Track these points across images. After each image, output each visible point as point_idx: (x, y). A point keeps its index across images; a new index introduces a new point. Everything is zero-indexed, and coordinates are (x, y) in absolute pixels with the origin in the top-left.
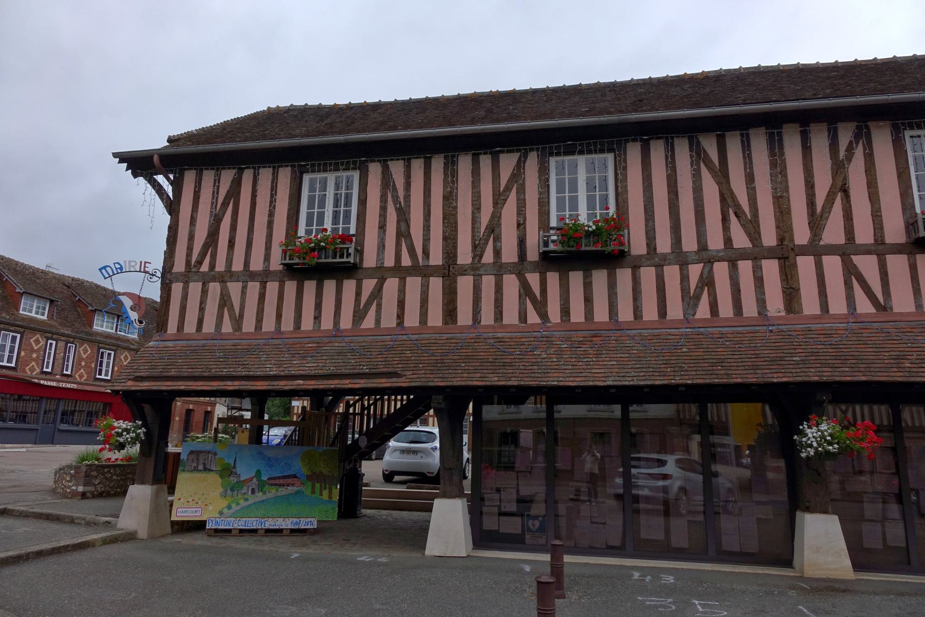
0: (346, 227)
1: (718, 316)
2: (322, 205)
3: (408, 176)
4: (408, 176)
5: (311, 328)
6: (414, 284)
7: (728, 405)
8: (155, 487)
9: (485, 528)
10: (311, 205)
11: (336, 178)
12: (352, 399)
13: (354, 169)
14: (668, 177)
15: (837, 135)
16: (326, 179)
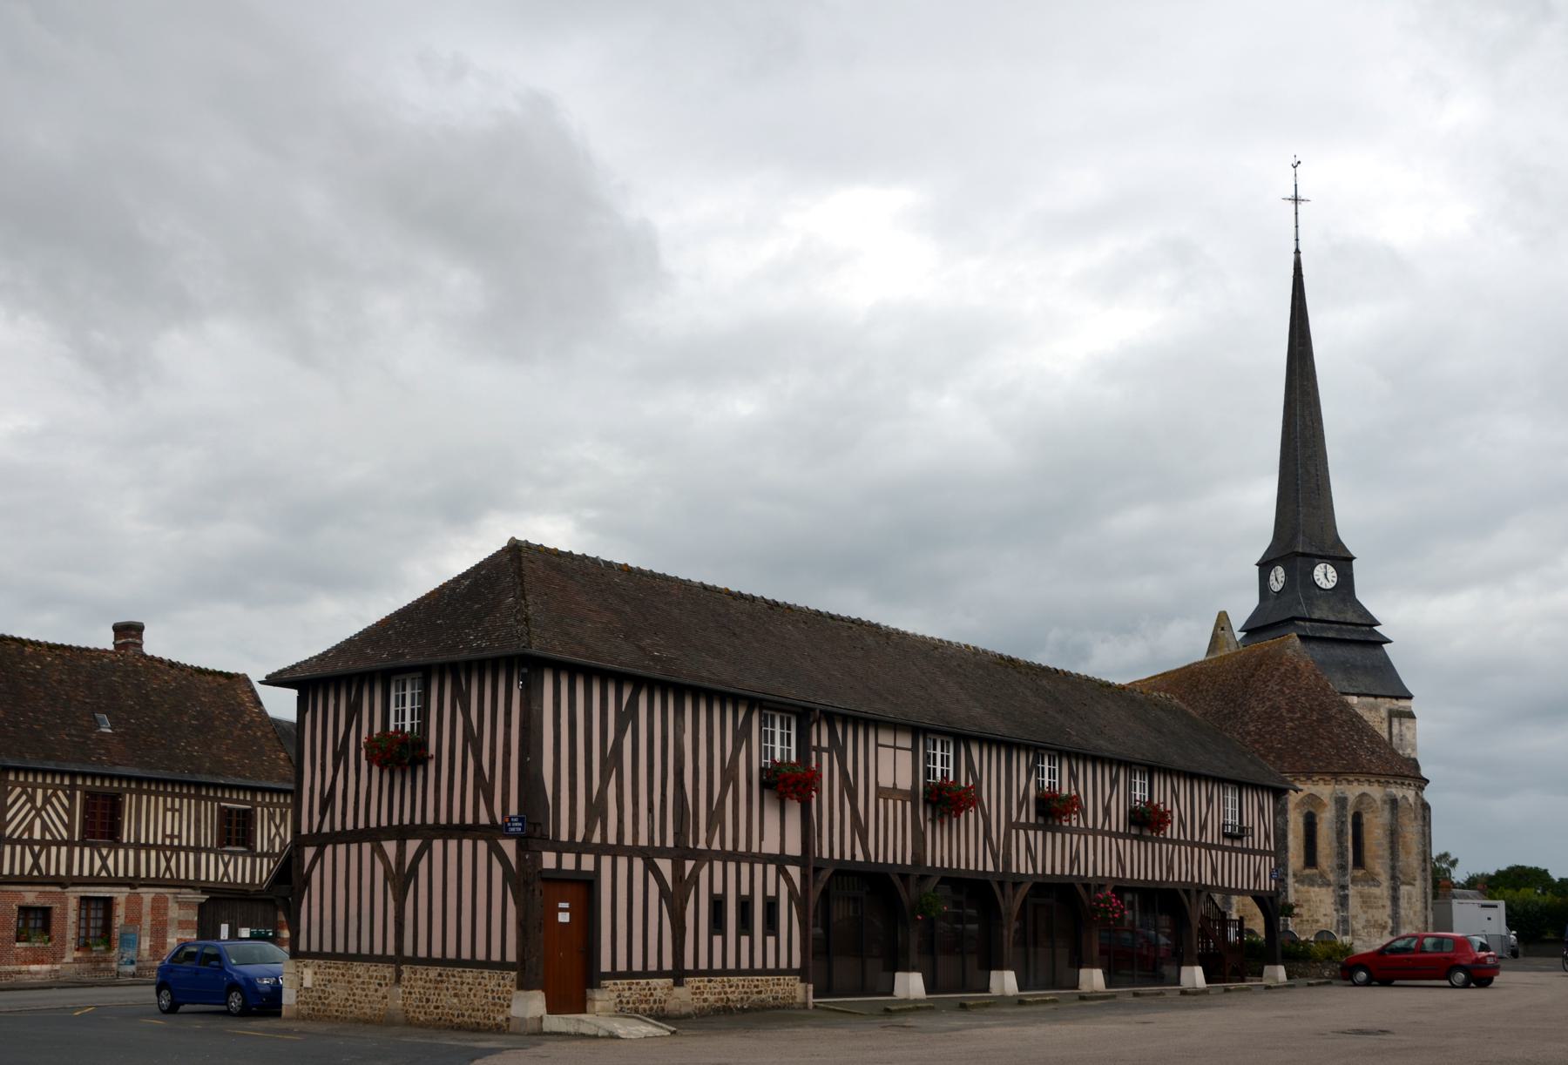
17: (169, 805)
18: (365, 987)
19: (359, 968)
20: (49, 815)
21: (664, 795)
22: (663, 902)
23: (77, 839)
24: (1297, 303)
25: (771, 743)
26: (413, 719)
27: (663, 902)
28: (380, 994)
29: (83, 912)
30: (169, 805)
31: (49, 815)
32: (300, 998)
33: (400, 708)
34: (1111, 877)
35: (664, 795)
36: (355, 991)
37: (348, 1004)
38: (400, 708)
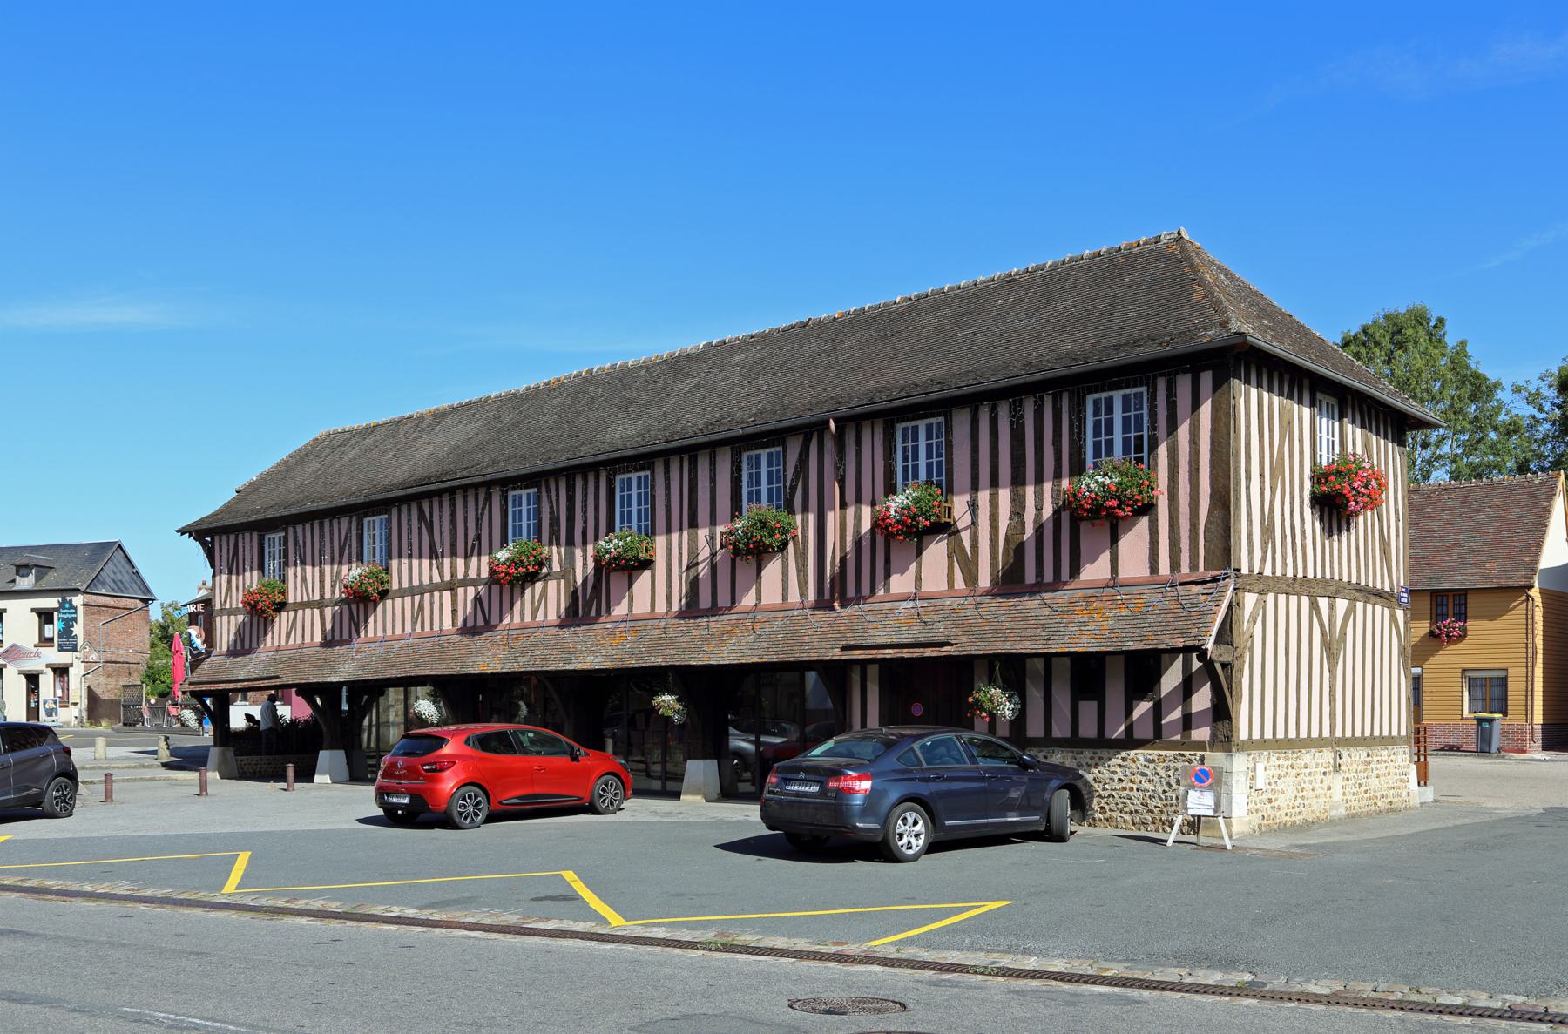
0: (1138, 457)
1: (1158, 573)
2: (1110, 431)
3: (431, 508)
4: (431, 508)
5: (1034, 582)
6: (308, 611)
7: (419, 688)
8: (221, 748)
9: (716, 761)
10: (1097, 433)
11: (528, 494)
12: (148, 701)
13: (1141, 385)
14: (711, 488)
15: (823, 440)
16: (760, 454)
17: (1439, 612)
18: (1312, 778)
19: (1307, 757)
20: (432, 603)
21: (1349, 566)
22: (956, 564)
23: (815, 789)
24: (1038, 443)
25: (628, 507)
26: (529, 519)
27: (956, 564)
28: (1325, 785)
29: (721, 612)
30: (1439, 612)
31: (432, 603)
32: (1251, 805)
33: (517, 523)
34: (1299, 595)
35: (1349, 566)
36: (1303, 785)
37: (1296, 804)
38: (517, 523)
